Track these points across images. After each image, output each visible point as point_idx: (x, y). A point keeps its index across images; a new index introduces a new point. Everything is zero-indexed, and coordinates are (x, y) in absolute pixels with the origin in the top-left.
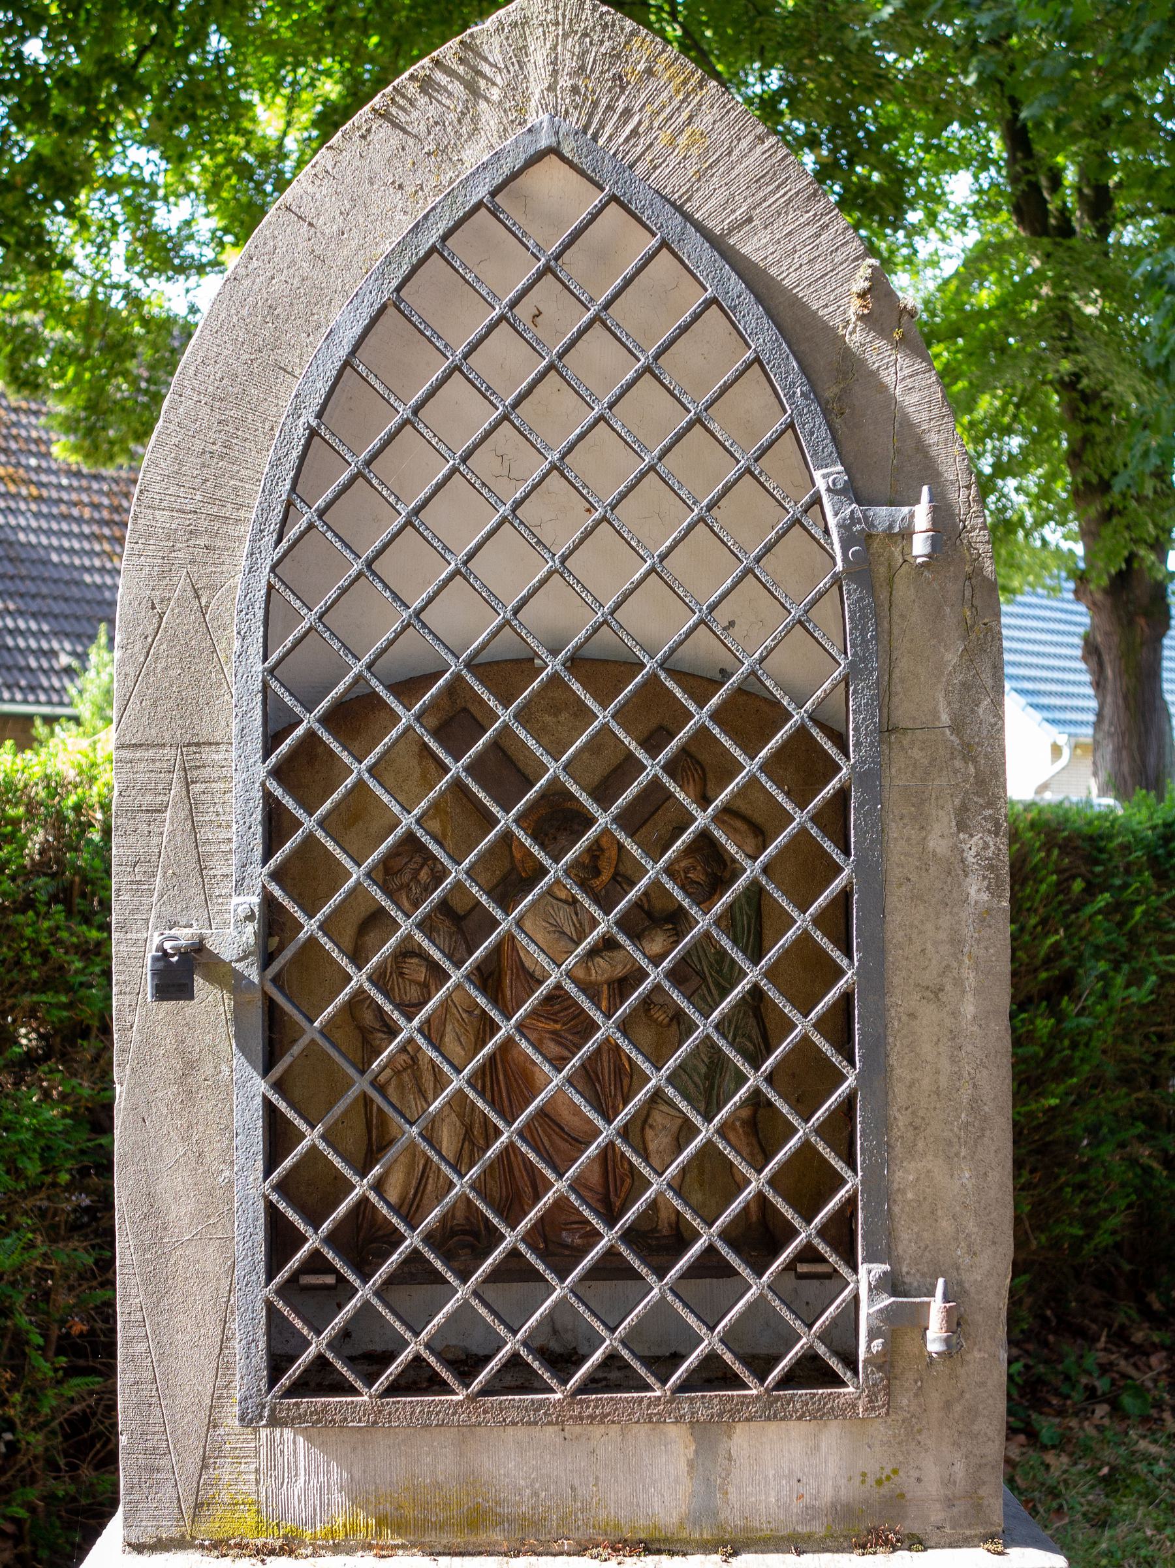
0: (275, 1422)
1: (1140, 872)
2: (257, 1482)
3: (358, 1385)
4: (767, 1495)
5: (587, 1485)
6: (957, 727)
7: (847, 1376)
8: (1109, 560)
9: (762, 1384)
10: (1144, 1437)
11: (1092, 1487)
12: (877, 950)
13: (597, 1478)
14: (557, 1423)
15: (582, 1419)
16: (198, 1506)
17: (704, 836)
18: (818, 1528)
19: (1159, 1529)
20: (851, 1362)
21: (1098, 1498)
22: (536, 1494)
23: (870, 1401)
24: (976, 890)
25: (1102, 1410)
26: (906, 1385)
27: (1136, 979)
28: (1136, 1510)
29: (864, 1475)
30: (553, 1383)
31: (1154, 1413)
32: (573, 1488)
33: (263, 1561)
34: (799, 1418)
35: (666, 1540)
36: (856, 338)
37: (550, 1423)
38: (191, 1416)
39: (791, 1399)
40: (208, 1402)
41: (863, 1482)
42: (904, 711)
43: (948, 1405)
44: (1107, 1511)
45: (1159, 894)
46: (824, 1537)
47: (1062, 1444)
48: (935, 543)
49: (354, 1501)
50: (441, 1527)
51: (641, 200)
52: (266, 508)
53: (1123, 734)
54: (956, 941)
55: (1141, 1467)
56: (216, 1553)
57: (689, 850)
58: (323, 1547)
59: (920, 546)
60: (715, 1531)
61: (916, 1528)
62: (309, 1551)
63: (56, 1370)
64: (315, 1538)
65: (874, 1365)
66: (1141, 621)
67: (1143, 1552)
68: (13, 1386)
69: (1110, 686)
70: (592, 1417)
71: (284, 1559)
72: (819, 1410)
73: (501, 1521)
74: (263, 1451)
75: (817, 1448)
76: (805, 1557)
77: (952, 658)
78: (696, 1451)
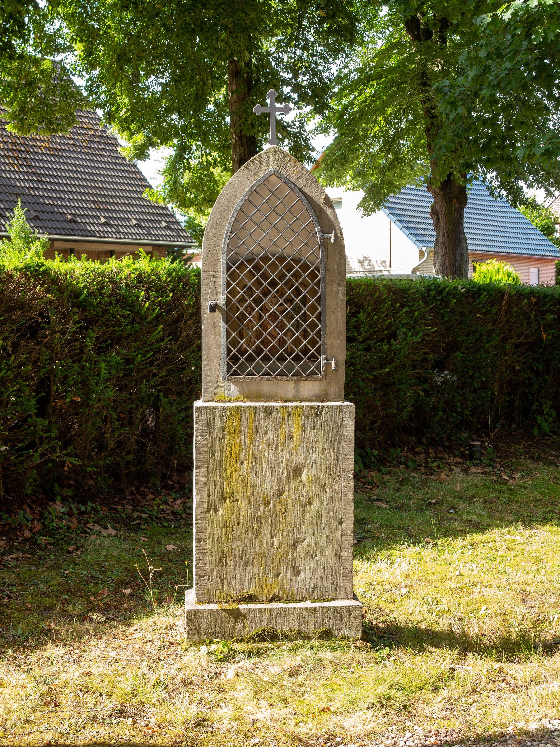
0: (228, 380)
1: (419, 301)
6: (338, 270)
8: (441, 175)
12: (324, 305)
17: (297, 287)
18: (314, 398)
20: (320, 372)
21: (397, 485)
24: (341, 296)
25: (402, 466)
27: (415, 334)
36: (322, 206)
42: (329, 267)
45: (424, 308)
47: (388, 473)
48: (335, 240)
51: (288, 183)
52: (227, 233)
53: (446, 248)
54: (337, 304)
55: (412, 479)
57: (294, 290)
59: (332, 241)
66: (455, 201)
69: (441, 228)
73: (264, 397)
77: (337, 258)
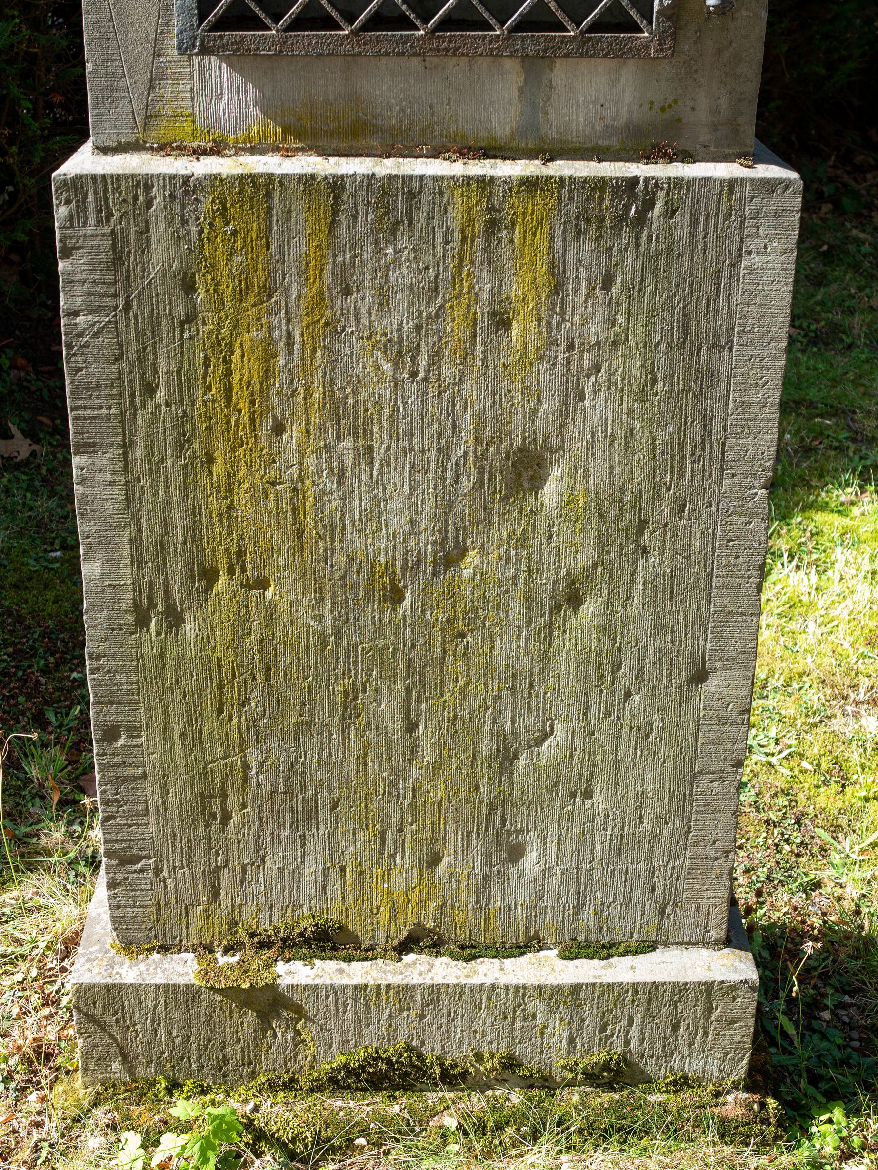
0: (204, 51)
2: (192, 99)
3: (268, 21)
4: (578, 116)
5: (442, 104)
7: (643, 24)
9: (578, 27)
10: (856, 228)
11: (814, 258)
13: (450, 99)
14: (420, 54)
15: (439, 51)
16: (148, 117)
18: (614, 143)
19: (860, 289)
22: (403, 110)
23: (660, 44)
25: (826, 208)
26: (689, 34)
28: (845, 275)
29: (652, 103)
30: (417, 22)
31: (865, 212)
32: (431, 107)
33: (198, 159)
34: (605, 56)
35: (500, 148)
37: (414, 54)
38: (140, 48)
39: (600, 40)
40: (153, 36)
41: (651, 108)
43: (719, 52)
44: (823, 275)
46: (620, 150)
49: (265, 113)
50: (331, 134)
55: (852, 248)
56: (162, 153)
58: (243, 149)
60: (537, 142)
61: (688, 145)
62: (232, 152)
63: (43, 129)
64: (236, 142)
65: (664, 15)
67: (847, 304)
68: (11, 141)
70: (447, 50)
71: (213, 158)
72: (620, 50)
74: (196, 74)
75: (617, 80)
76: (604, 164)
78: (525, 80)
